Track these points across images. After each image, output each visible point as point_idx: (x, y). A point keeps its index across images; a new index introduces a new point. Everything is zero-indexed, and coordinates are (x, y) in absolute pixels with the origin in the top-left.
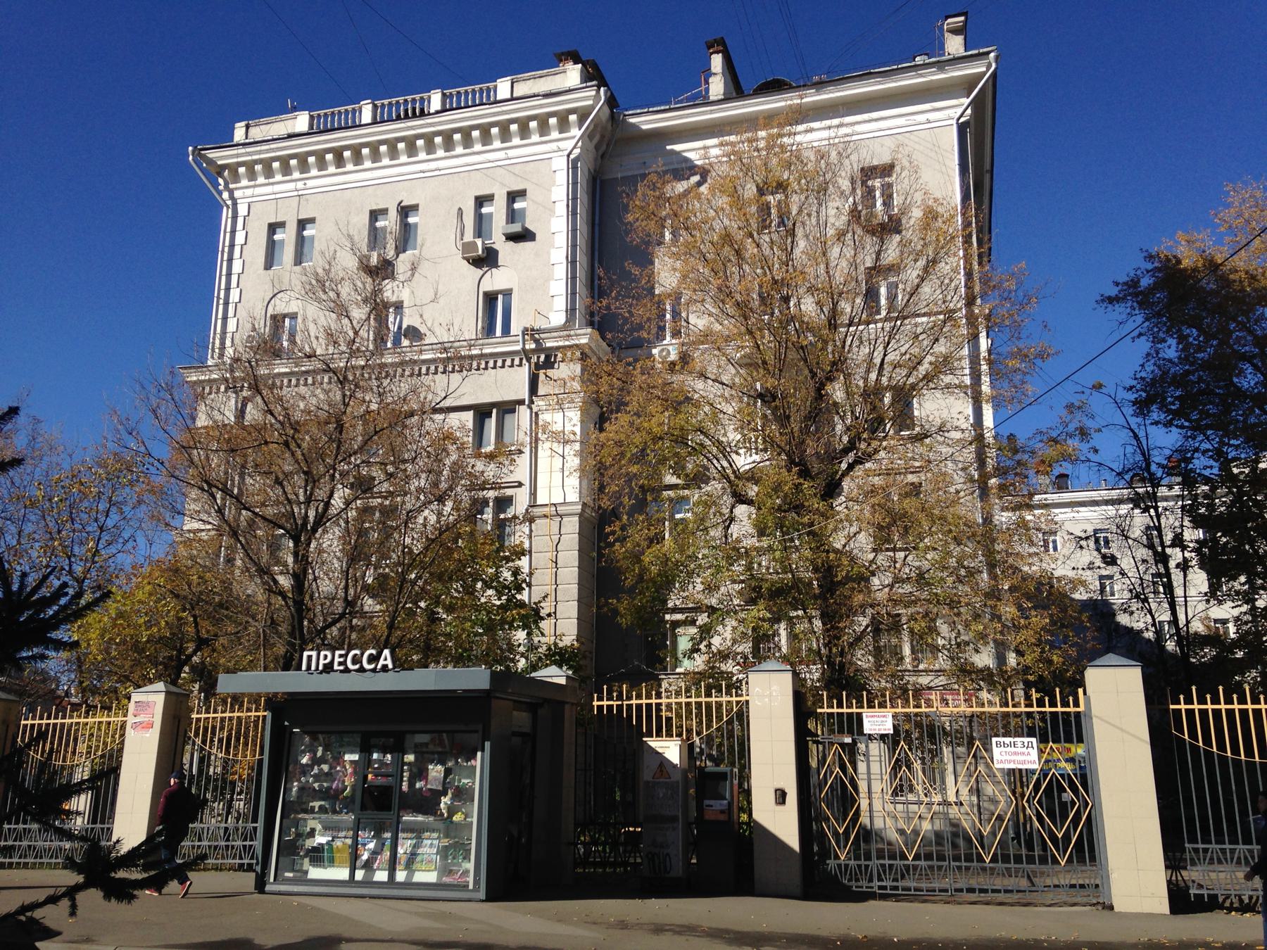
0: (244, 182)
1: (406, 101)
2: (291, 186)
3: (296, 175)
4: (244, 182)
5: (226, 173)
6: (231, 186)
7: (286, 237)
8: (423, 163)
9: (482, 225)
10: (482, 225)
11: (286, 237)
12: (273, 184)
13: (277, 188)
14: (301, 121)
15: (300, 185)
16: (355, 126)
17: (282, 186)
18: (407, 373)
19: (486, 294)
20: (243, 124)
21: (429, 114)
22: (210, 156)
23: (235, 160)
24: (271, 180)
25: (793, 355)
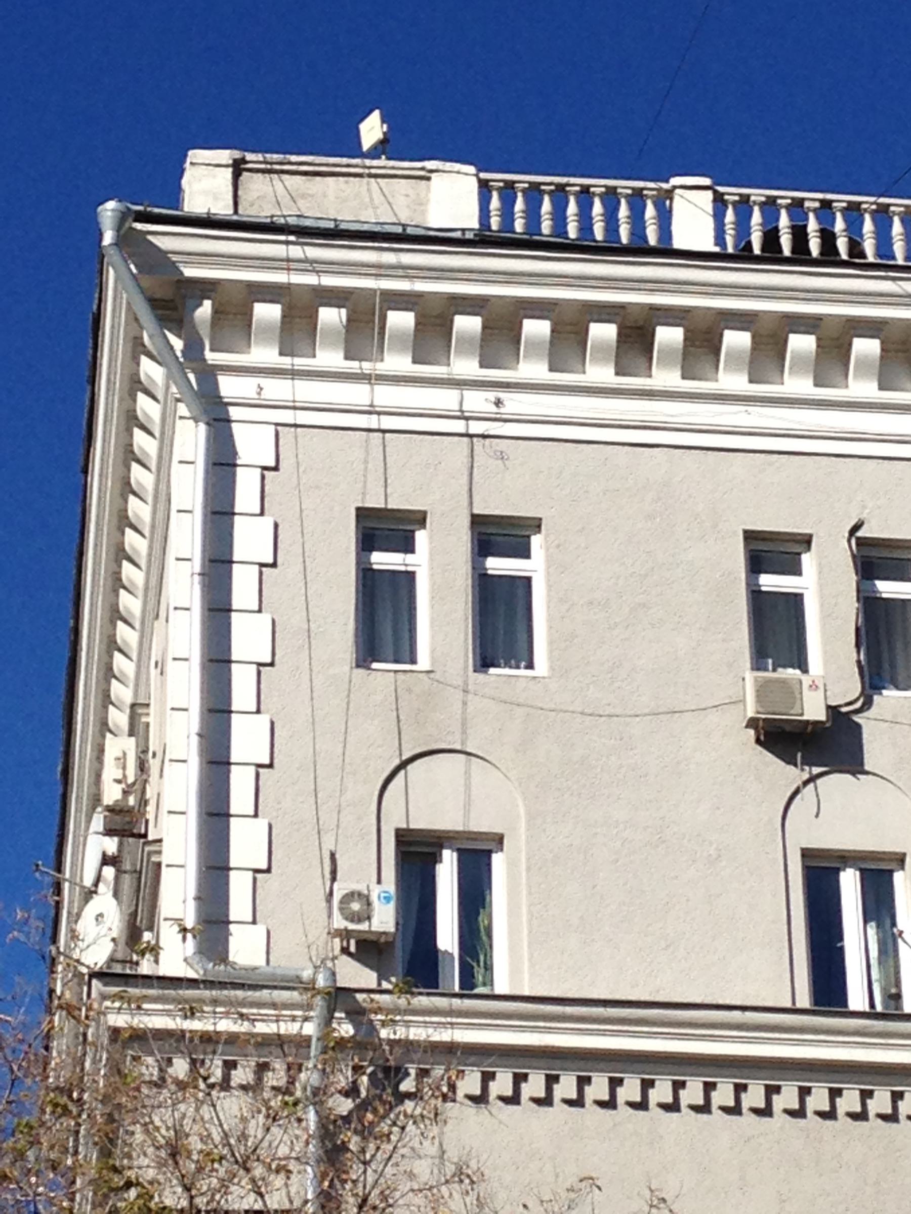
0: (264, 354)
1: (826, 205)
2: (447, 399)
3: (465, 366)
4: (264, 354)
5: (205, 309)
6: (211, 357)
7: (437, 569)
8: (592, 399)
9: (776, 629)
10: (776, 629)
11: (437, 569)
12: (294, 374)
13: (386, 396)
14: (451, 196)
15: (478, 401)
16: (638, 249)
17: (405, 391)
18: (780, 1102)
19: (404, 838)
20: (225, 156)
21: (666, 251)
22: (163, 243)
23: (311, 279)
24: (300, 362)
25: (70, 1175)
